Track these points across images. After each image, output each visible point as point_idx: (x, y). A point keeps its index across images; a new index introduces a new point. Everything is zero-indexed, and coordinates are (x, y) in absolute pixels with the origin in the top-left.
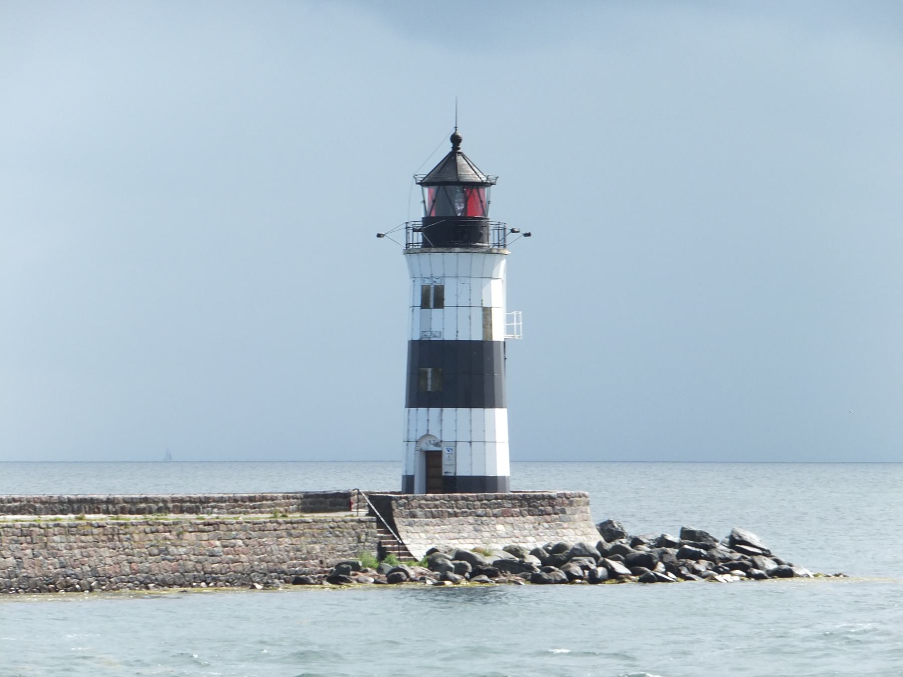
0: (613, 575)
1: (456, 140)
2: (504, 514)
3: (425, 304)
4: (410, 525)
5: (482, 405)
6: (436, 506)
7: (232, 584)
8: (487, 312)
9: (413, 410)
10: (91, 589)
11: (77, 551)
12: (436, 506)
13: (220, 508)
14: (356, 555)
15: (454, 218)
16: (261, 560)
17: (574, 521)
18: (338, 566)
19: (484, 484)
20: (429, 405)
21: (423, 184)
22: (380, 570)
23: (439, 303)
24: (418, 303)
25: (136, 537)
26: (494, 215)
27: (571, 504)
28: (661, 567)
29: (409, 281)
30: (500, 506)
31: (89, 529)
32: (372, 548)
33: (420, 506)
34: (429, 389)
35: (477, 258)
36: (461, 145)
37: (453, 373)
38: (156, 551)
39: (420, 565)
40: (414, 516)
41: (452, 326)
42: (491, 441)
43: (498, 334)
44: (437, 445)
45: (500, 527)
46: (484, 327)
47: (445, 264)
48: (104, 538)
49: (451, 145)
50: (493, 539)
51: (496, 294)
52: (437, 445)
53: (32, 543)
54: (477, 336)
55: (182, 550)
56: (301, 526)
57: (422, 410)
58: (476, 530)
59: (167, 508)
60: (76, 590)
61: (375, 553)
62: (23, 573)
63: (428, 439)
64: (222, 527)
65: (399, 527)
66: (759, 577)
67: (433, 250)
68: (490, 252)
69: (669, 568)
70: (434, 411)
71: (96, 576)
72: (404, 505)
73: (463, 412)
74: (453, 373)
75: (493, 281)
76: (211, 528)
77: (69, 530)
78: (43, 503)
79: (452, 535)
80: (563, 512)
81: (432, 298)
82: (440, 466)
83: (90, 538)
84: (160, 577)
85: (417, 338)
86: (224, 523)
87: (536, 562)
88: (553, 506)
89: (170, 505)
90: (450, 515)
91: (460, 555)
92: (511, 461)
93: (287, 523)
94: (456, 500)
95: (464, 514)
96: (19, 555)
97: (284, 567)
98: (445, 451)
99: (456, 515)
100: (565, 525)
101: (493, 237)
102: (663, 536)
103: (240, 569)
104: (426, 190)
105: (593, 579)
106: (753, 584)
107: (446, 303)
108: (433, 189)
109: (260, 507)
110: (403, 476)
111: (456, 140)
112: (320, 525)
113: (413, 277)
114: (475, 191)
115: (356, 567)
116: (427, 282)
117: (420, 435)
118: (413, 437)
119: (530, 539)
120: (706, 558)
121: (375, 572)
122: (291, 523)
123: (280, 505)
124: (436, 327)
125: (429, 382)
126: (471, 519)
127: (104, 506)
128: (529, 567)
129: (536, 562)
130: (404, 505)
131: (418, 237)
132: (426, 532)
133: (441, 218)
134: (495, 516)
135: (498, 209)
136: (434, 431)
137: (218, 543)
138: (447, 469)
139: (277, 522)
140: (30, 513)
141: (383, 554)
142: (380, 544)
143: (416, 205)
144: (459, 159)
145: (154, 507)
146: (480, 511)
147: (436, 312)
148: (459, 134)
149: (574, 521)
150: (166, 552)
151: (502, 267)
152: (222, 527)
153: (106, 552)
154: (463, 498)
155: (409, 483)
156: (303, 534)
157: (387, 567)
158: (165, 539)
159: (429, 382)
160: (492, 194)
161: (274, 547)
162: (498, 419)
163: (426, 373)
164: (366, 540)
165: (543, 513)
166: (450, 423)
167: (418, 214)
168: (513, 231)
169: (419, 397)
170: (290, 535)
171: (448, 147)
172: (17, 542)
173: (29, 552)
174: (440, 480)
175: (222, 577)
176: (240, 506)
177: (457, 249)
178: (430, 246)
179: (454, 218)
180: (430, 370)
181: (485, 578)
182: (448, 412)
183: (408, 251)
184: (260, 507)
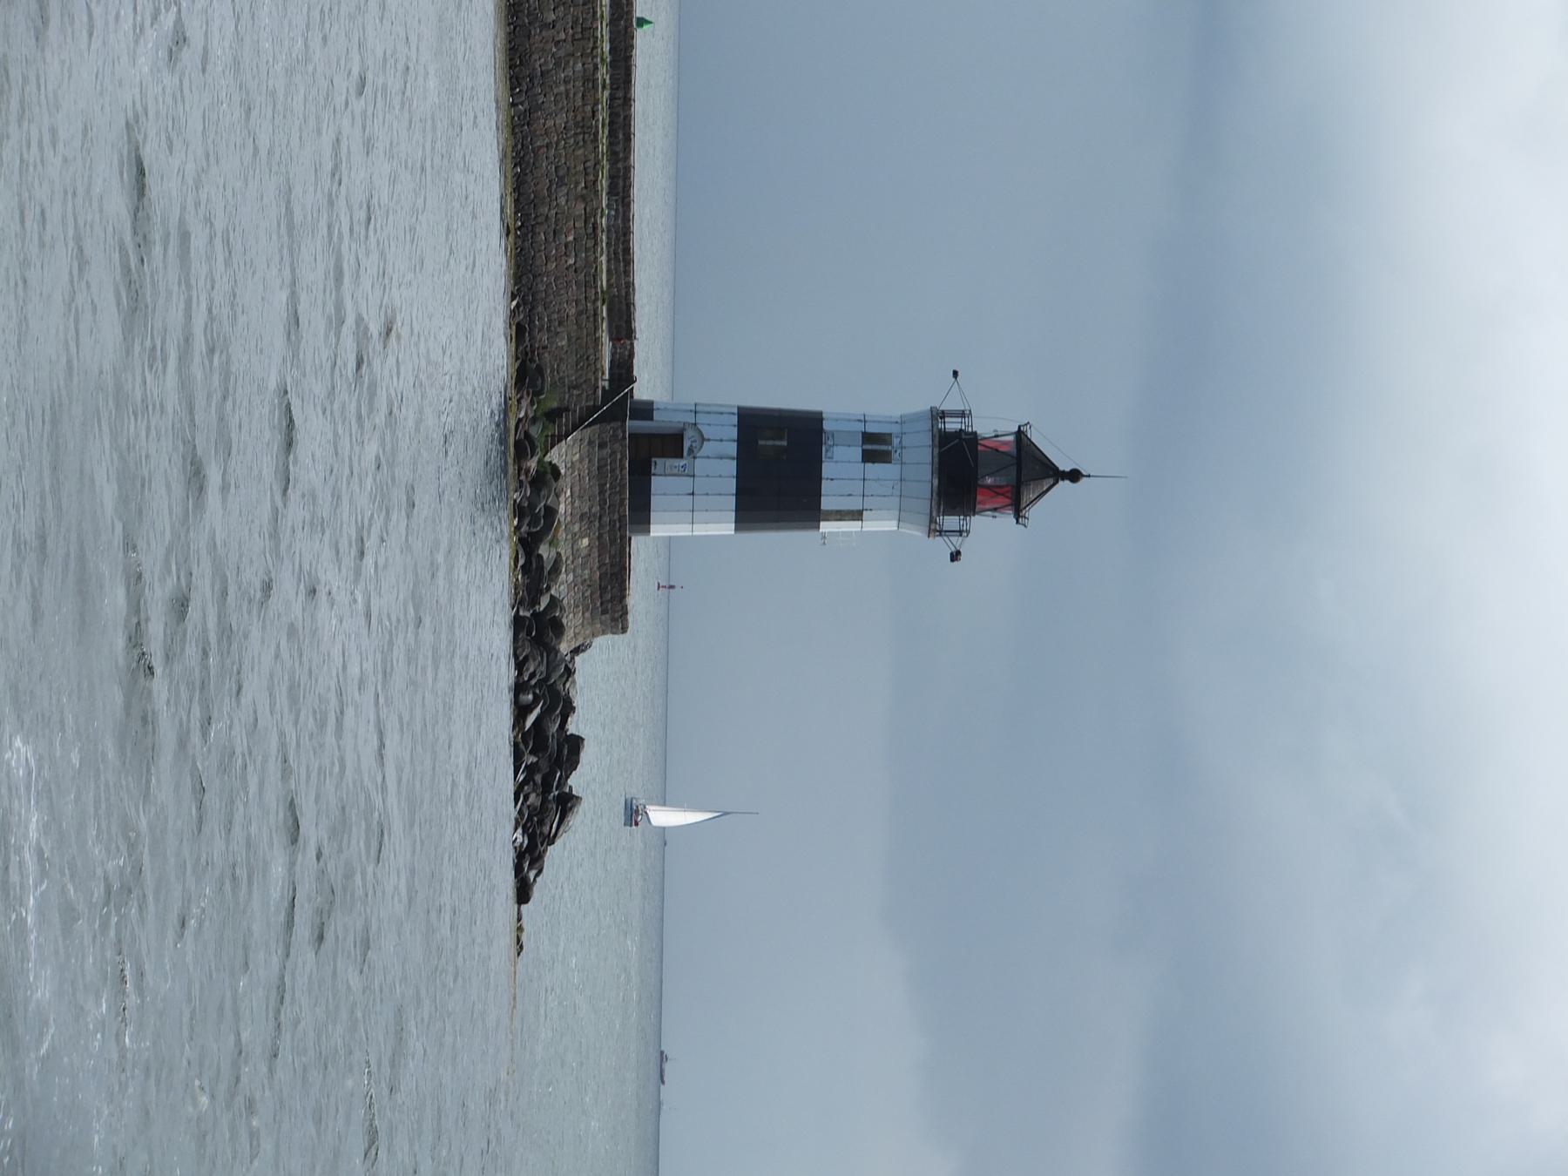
0: (520, 712)
1: (1074, 476)
2: (601, 547)
3: (868, 438)
4: (590, 443)
5: (740, 509)
6: (613, 470)
7: (517, 255)
8: (857, 515)
9: (735, 419)
10: (513, 105)
11: (562, 88)
12: (613, 470)
13: (616, 218)
14: (553, 384)
15: (978, 474)
16: (549, 285)
17: (592, 624)
18: (540, 370)
19: (641, 516)
20: (741, 441)
21: (1020, 434)
22: (534, 420)
23: (868, 457)
24: (871, 429)
25: (580, 152)
26: (981, 524)
27: (614, 620)
28: (532, 759)
29: (896, 413)
30: (613, 541)
31: (591, 101)
32: (562, 400)
33: (613, 453)
34: (761, 442)
35: (925, 505)
36: (1067, 482)
37: (781, 469)
38: (561, 173)
39: (540, 462)
40: (602, 446)
41: (840, 471)
42: (691, 525)
43: (826, 527)
44: (691, 450)
45: (586, 541)
46: (838, 512)
47: (919, 459)
48: (579, 118)
49: (1068, 469)
50: (570, 545)
51: (880, 524)
52: (691, 450)
53: (574, 40)
54: (827, 503)
55: (562, 201)
56: (591, 325)
57: (734, 433)
58: (582, 516)
59: (617, 162)
60: (512, 89)
61: (555, 405)
62: (535, 31)
63: (697, 437)
64: (590, 243)
65: (589, 430)
66: (518, 869)
67: (936, 451)
68: (932, 521)
69: (531, 769)
70: (732, 449)
71: (530, 111)
72: (615, 436)
73: (732, 485)
74: (781, 469)
75: (895, 523)
76: (590, 230)
77: (589, 79)
78: (626, 28)
79: (577, 489)
80: (604, 612)
81: (876, 448)
82: (663, 455)
83: (579, 103)
84: (529, 178)
85: (826, 426)
86: (596, 244)
87: (544, 602)
88: (611, 600)
89: (620, 165)
90: (602, 486)
91: (551, 512)
92: (664, 804)
93: (595, 310)
94: (621, 492)
95: (602, 503)
96: (558, 26)
97: (540, 309)
98: (682, 462)
99: (602, 492)
100: (587, 615)
101: (951, 522)
102: (578, 799)
103: (538, 263)
104: (1011, 438)
105: (519, 688)
106: (509, 859)
107: (869, 465)
108: (1012, 449)
109: (617, 259)
110: (652, 403)
111: (1074, 476)
112: (591, 345)
113: (902, 421)
114: (1008, 501)
115: (537, 393)
116: (896, 441)
117: (704, 429)
118: (701, 419)
119: (571, 577)
120: (544, 801)
121: (531, 415)
122: (595, 314)
123: (618, 279)
124: (839, 452)
125: (770, 443)
126: (596, 509)
127: (620, 94)
128: (535, 601)
129: (544, 602)
130: (615, 436)
131: (952, 425)
132: (581, 460)
133: (976, 459)
134: (600, 537)
135: (989, 530)
136: (708, 448)
137: (571, 238)
138: (660, 464)
139: (596, 299)
140: (612, 15)
141: (552, 416)
142: (567, 409)
143: (992, 422)
144: (1051, 481)
145: (619, 148)
146: (606, 519)
147: (857, 453)
148: (1084, 480)
149: (592, 624)
150: (561, 182)
151: (916, 533)
152: (590, 243)
153: (561, 120)
154: (622, 501)
155: (645, 410)
156: (580, 327)
157: (535, 431)
158: (577, 183)
159: (770, 443)
160: (1007, 519)
161: (565, 298)
162: (728, 528)
163: (781, 439)
164: (571, 396)
165: (603, 590)
166: (717, 466)
167: (983, 426)
168: (955, 556)
169: (755, 426)
170: (580, 313)
171: (1064, 466)
172: (575, 22)
173: (563, 36)
174: (644, 452)
175: (526, 244)
176: (617, 239)
177: (936, 482)
178: (940, 446)
179: (978, 474)
180: (784, 443)
181: (521, 562)
182: (732, 467)
183: (939, 415)
184: (617, 259)
